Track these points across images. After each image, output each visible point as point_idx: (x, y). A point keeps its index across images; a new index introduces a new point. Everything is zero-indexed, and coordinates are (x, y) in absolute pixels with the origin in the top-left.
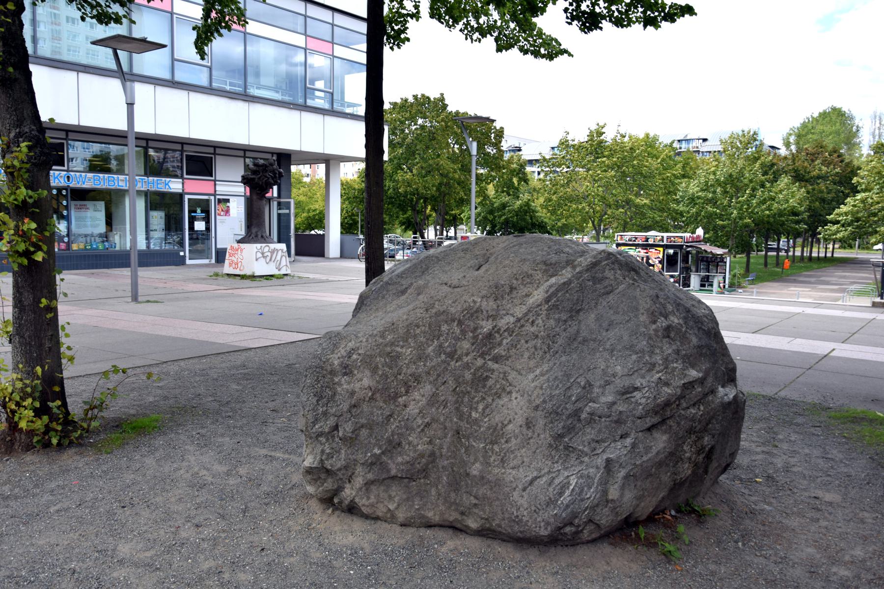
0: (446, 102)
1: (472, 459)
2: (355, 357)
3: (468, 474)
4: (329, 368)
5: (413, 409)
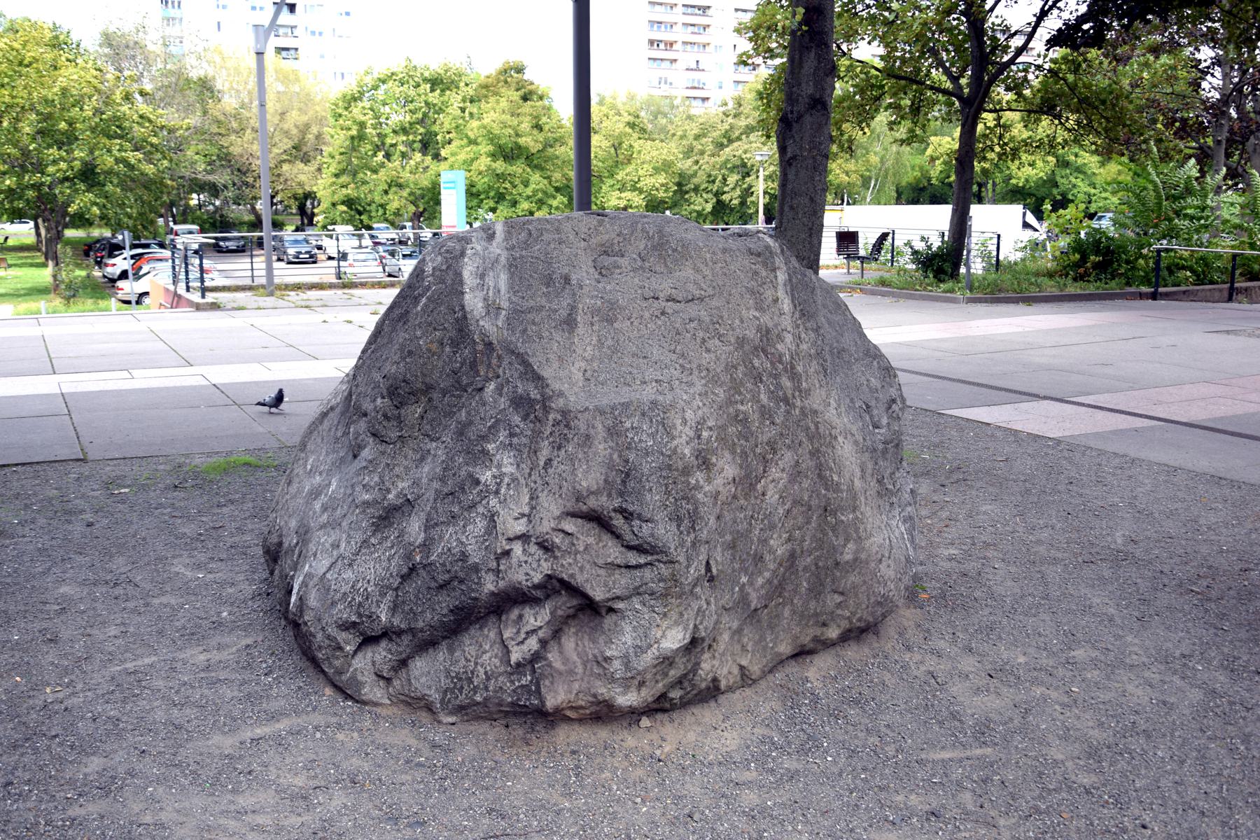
0: (485, 67)
1: (841, 541)
2: (705, 434)
3: (837, 564)
4: (680, 464)
5: (772, 497)
